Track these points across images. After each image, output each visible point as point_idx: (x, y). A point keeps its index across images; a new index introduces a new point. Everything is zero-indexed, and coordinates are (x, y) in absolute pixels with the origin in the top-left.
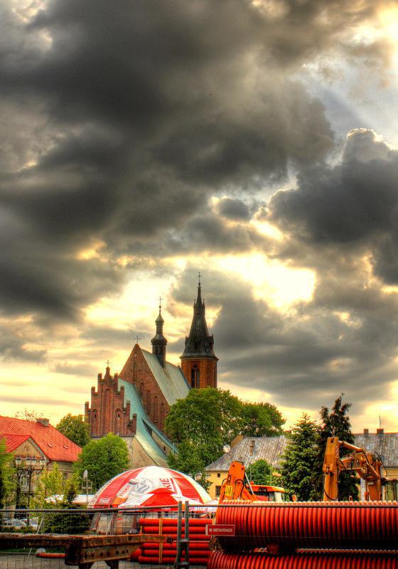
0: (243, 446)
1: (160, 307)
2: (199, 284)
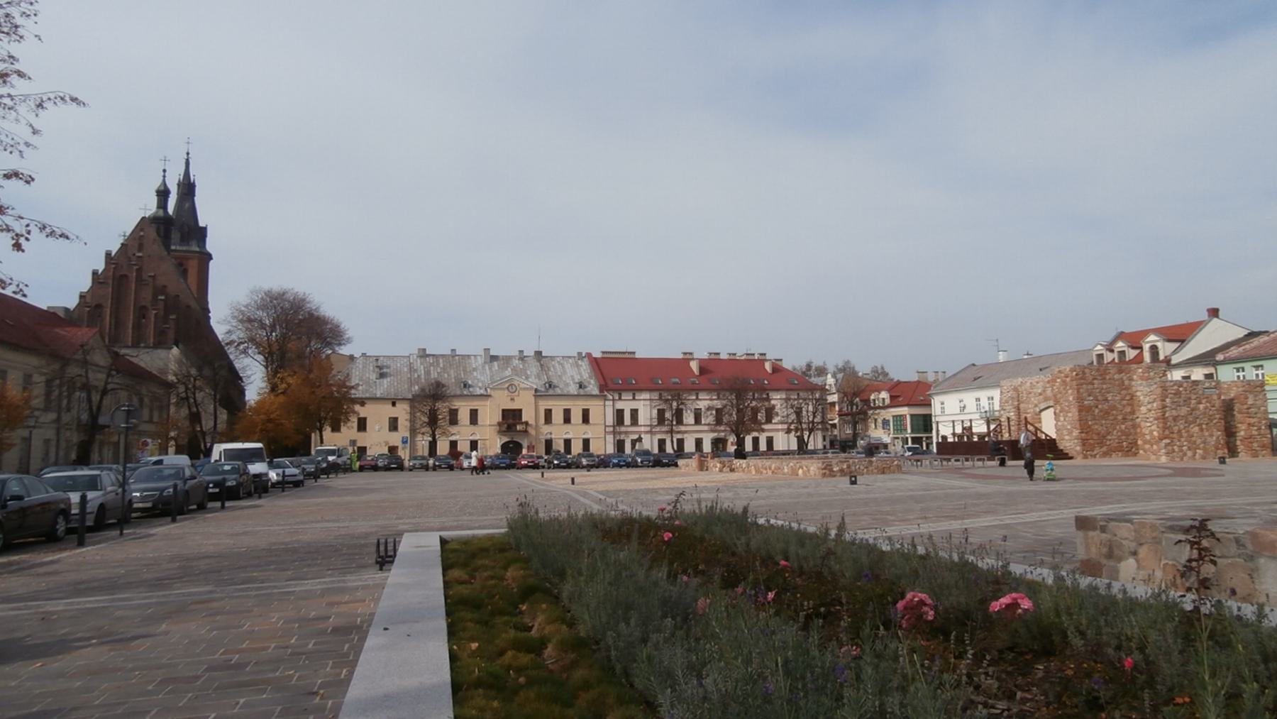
0: (361, 366)
1: (164, 171)
2: (188, 154)
